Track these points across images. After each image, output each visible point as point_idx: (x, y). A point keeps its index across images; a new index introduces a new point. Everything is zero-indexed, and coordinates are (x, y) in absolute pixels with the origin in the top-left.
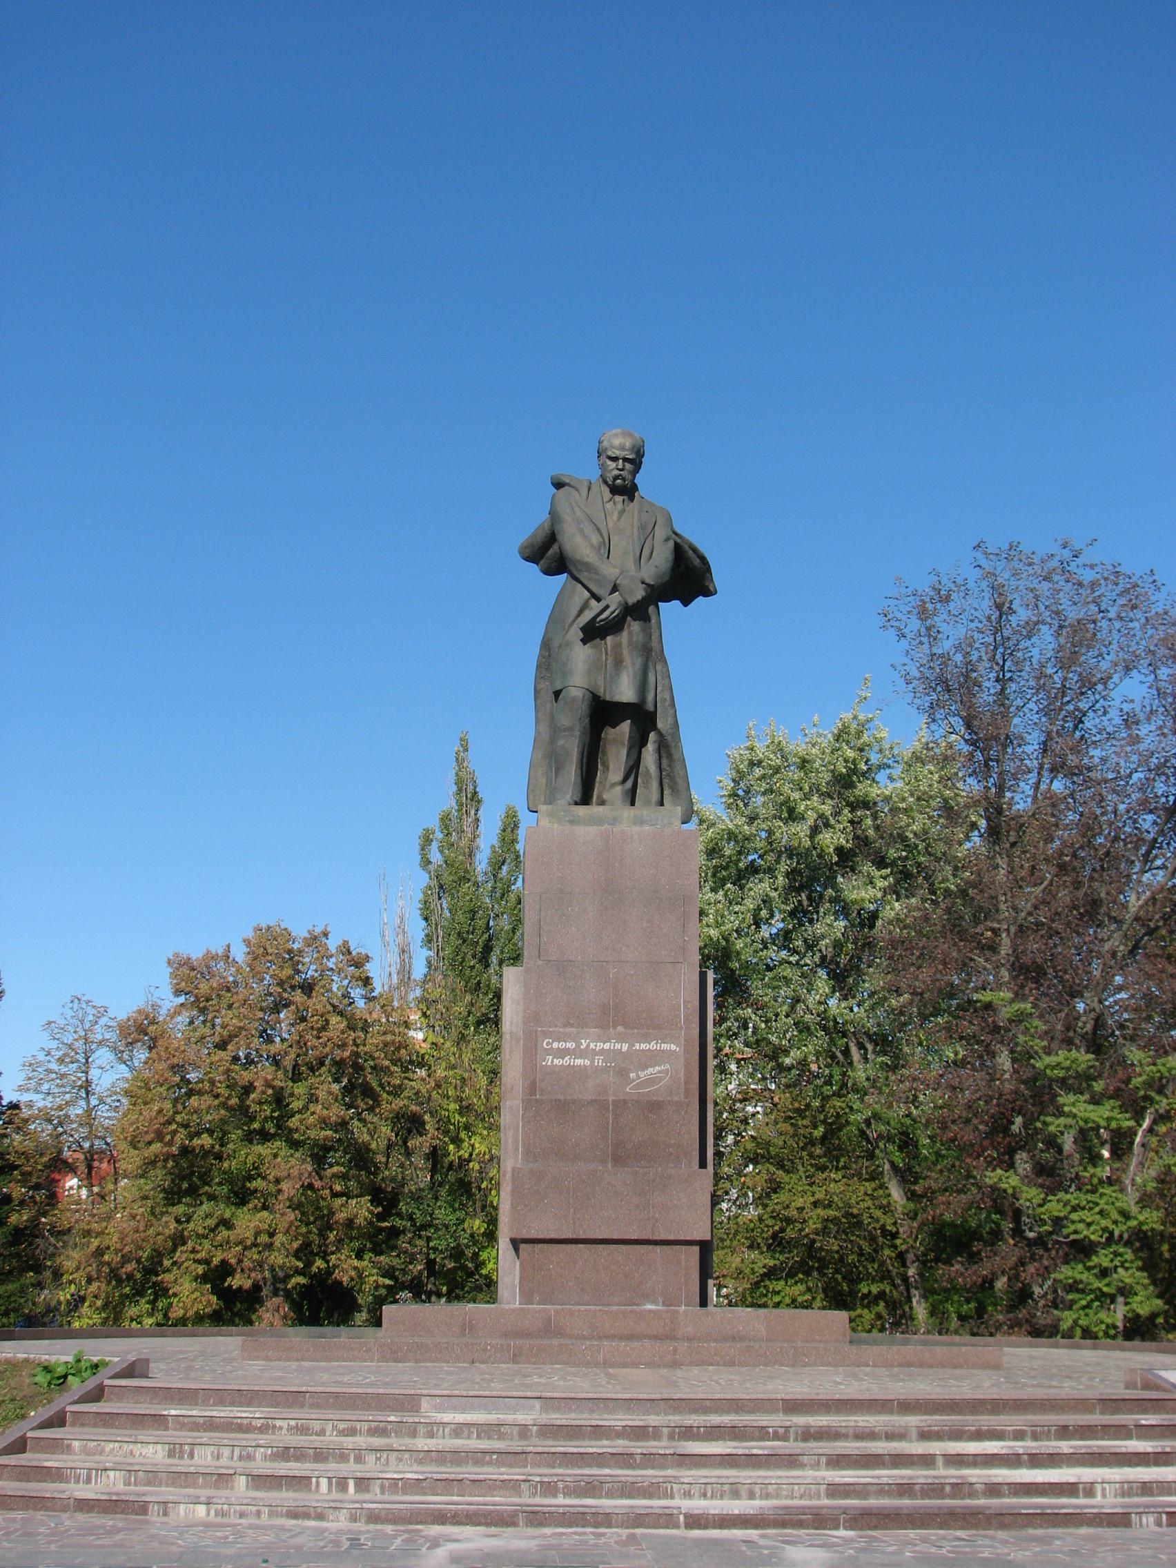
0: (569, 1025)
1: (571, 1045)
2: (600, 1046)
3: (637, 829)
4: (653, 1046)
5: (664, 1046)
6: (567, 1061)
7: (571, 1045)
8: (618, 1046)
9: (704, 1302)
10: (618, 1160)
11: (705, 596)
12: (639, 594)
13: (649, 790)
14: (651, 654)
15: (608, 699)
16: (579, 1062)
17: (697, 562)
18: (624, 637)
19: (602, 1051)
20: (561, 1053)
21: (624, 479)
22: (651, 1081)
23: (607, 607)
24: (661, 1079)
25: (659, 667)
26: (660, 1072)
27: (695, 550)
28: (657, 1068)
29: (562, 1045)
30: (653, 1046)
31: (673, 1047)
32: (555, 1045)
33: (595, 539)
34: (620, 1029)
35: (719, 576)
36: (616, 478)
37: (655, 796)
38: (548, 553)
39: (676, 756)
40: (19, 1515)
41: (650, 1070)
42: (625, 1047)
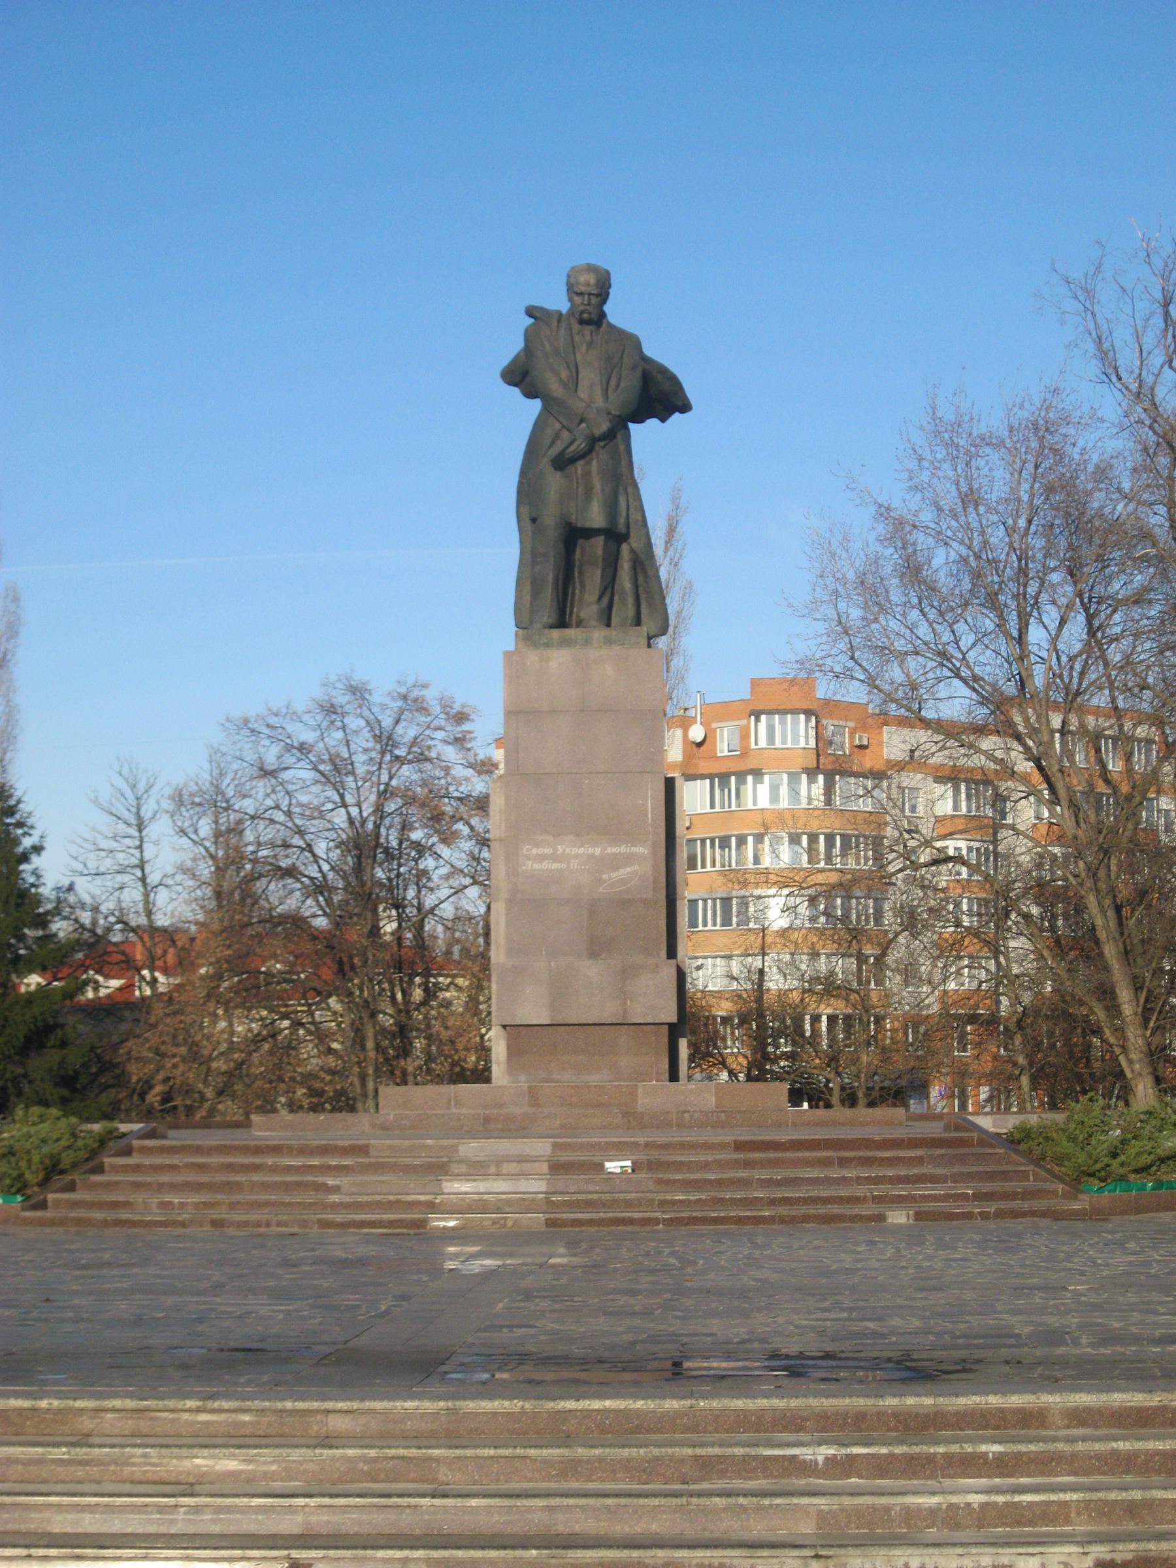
2: (575, 851)
5: (634, 849)
6: (545, 865)
7: (548, 851)
8: (591, 850)
9: (674, 1076)
13: (623, 610)
14: (622, 480)
15: (579, 525)
16: (555, 866)
19: (577, 856)
20: (541, 858)
22: (623, 881)
25: (630, 490)
27: (663, 370)
29: (540, 851)
31: (642, 850)
37: (631, 612)
38: (520, 376)
40: (72, 1516)
41: (622, 871)
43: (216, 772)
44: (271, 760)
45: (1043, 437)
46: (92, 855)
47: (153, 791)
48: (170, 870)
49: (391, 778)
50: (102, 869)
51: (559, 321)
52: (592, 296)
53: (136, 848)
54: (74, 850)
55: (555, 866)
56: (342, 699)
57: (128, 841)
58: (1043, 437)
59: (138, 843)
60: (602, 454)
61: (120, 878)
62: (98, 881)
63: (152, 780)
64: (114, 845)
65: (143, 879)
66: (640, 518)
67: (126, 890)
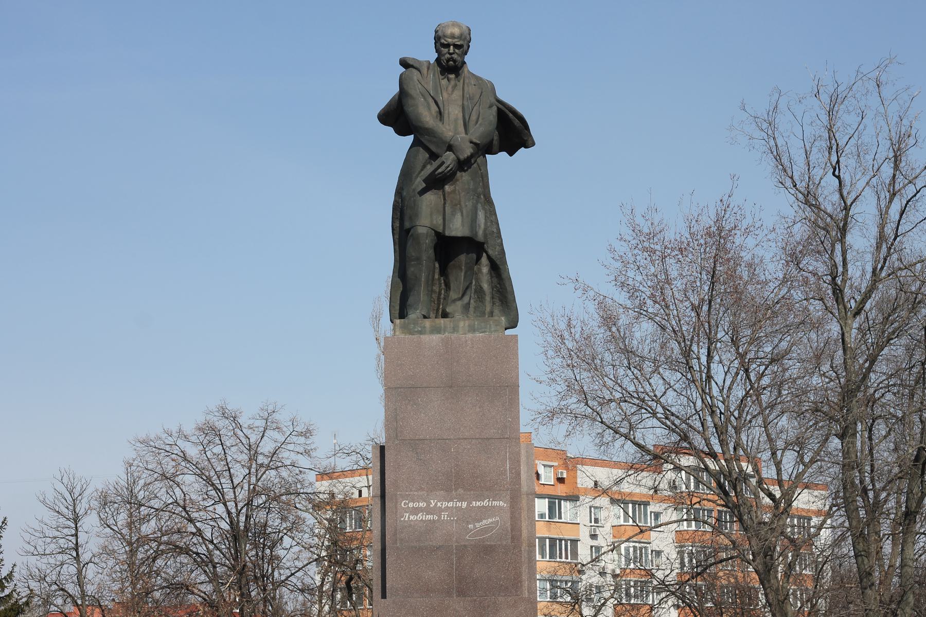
0: (422, 489)
1: (422, 505)
2: (445, 504)
3: (470, 335)
4: (486, 503)
5: (495, 503)
6: (420, 516)
7: (422, 505)
8: (459, 504)
10: (461, 593)
11: (526, 147)
12: (468, 151)
16: (430, 517)
17: (516, 122)
18: (459, 186)
19: (447, 508)
20: (415, 511)
21: (455, 61)
23: (443, 163)
24: (493, 528)
26: (492, 523)
27: (515, 113)
28: (490, 520)
29: (416, 505)
30: (486, 503)
32: (411, 505)
33: (434, 108)
34: (461, 491)
35: (535, 131)
36: (448, 60)
38: (397, 116)
39: (504, 276)
41: (484, 522)
42: (465, 505)
43: (131, 480)
44: (170, 469)
45: (717, 246)
46: (40, 542)
47: (86, 494)
48: (96, 550)
49: (258, 480)
50: (47, 552)
51: (428, 68)
52: (451, 58)
53: (72, 536)
54: (27, 537)
55: (430, 517)
56: (221, 424)
57: (66, 531)
58: (717, 246)
59: (74, 532)
60: (464, 177)
61: (60, 557)
62: (45, 560)
63: (85, 486)
64: (57, 534)
65: (77, 558)
66: (495, 230)
67: (65, 566)
